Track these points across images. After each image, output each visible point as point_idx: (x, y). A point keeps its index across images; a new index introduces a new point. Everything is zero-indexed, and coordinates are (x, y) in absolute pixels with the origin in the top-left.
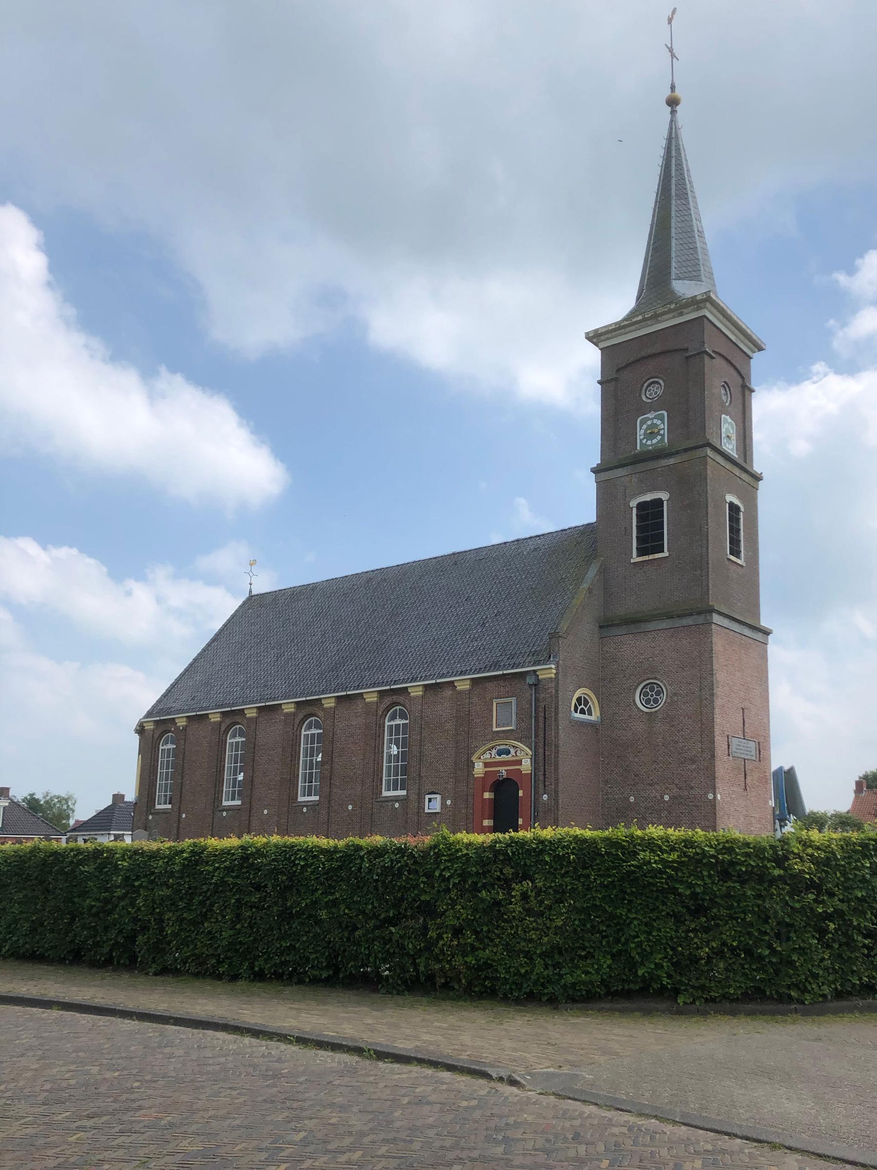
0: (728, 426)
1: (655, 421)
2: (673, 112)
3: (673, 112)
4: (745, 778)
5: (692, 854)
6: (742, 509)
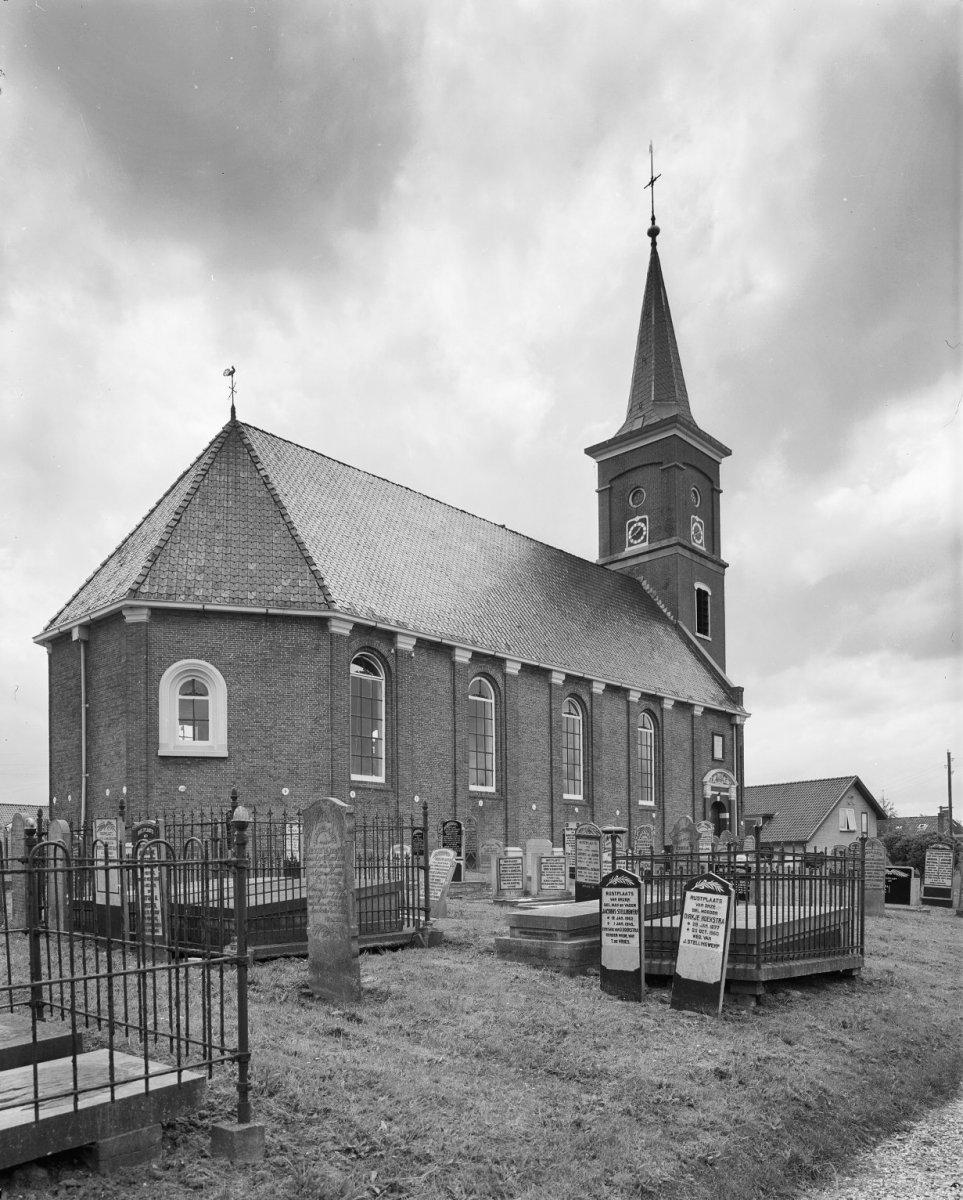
0: (697, 523)
2: (654, 244)
3: (654, 244)
4: (629, 799)
5: (149, 934)
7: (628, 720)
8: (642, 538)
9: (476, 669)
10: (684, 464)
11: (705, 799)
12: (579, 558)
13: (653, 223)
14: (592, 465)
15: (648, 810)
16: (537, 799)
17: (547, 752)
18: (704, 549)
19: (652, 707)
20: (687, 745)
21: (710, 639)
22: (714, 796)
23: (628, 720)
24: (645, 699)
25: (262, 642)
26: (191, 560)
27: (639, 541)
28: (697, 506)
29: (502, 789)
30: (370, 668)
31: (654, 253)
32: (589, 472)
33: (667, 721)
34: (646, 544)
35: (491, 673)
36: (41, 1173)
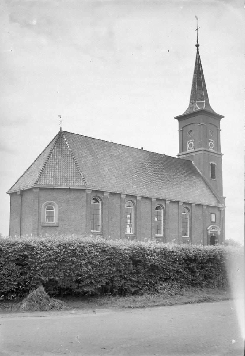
2: (198, 49)
3: (198, 49)
8: (192, 147)
10: (206, 123)
11: (208, 235)
13: (197, 43)
16: (147, 236)
19: (187, 206)
20: (201, 218)
25: (68, 196)
26: (50, 174)
28: (212, 136)
29: (164, 235)
30: (97, 201)
31: (198, 53)
34: (194, 149)
35: (133, 200)
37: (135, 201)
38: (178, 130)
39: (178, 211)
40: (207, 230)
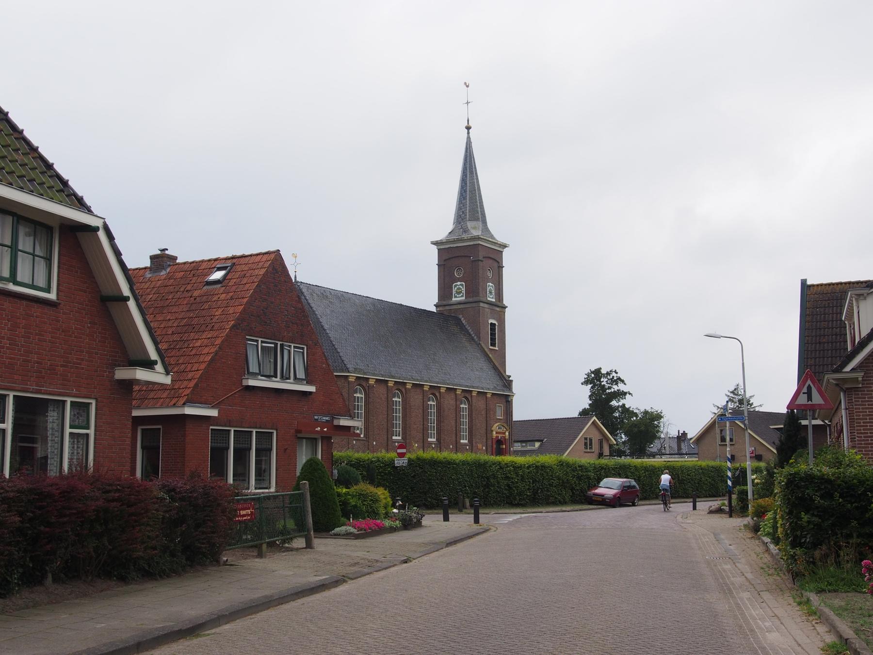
0: (490, 286)
1: (460, 286)
2: (468, 133)
3: (468, 133)
4: (456, 440)
6: (497, 324)
7: (456, 403)
9: (395, 387)
12: (429, 311)
13: (468, 123)
14: (434, 250)
15: (465, 445)
17: (422, 420)
18: (494, 300)
20: (483, 412)
21: (497, 349)
22: (497, 437)
23: (456, 403)
24: (464, 392)
27: (460, 295)
31: (469, 138)
32: (433, 254)
33: (474, 401)
35: (401, 389)
36: (816, 477)
37: (403, 390)
38: (437, 263)
39: (455, 403)
40: (492, 431)
